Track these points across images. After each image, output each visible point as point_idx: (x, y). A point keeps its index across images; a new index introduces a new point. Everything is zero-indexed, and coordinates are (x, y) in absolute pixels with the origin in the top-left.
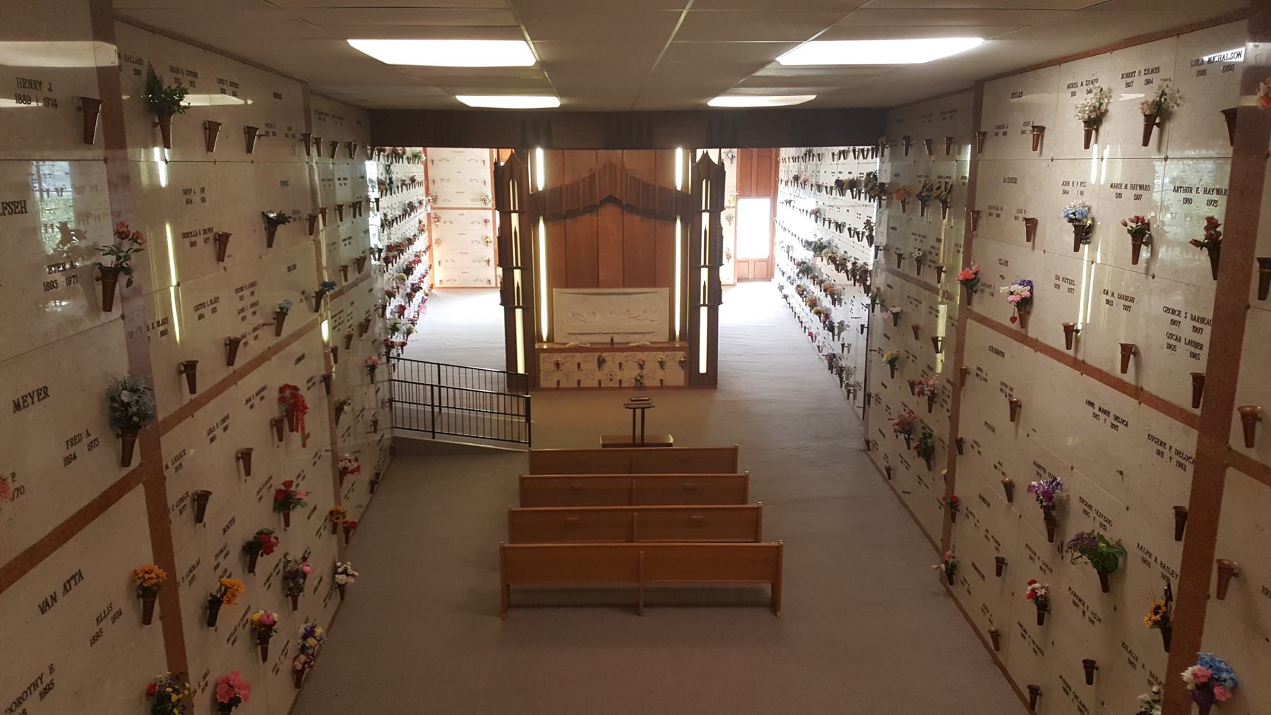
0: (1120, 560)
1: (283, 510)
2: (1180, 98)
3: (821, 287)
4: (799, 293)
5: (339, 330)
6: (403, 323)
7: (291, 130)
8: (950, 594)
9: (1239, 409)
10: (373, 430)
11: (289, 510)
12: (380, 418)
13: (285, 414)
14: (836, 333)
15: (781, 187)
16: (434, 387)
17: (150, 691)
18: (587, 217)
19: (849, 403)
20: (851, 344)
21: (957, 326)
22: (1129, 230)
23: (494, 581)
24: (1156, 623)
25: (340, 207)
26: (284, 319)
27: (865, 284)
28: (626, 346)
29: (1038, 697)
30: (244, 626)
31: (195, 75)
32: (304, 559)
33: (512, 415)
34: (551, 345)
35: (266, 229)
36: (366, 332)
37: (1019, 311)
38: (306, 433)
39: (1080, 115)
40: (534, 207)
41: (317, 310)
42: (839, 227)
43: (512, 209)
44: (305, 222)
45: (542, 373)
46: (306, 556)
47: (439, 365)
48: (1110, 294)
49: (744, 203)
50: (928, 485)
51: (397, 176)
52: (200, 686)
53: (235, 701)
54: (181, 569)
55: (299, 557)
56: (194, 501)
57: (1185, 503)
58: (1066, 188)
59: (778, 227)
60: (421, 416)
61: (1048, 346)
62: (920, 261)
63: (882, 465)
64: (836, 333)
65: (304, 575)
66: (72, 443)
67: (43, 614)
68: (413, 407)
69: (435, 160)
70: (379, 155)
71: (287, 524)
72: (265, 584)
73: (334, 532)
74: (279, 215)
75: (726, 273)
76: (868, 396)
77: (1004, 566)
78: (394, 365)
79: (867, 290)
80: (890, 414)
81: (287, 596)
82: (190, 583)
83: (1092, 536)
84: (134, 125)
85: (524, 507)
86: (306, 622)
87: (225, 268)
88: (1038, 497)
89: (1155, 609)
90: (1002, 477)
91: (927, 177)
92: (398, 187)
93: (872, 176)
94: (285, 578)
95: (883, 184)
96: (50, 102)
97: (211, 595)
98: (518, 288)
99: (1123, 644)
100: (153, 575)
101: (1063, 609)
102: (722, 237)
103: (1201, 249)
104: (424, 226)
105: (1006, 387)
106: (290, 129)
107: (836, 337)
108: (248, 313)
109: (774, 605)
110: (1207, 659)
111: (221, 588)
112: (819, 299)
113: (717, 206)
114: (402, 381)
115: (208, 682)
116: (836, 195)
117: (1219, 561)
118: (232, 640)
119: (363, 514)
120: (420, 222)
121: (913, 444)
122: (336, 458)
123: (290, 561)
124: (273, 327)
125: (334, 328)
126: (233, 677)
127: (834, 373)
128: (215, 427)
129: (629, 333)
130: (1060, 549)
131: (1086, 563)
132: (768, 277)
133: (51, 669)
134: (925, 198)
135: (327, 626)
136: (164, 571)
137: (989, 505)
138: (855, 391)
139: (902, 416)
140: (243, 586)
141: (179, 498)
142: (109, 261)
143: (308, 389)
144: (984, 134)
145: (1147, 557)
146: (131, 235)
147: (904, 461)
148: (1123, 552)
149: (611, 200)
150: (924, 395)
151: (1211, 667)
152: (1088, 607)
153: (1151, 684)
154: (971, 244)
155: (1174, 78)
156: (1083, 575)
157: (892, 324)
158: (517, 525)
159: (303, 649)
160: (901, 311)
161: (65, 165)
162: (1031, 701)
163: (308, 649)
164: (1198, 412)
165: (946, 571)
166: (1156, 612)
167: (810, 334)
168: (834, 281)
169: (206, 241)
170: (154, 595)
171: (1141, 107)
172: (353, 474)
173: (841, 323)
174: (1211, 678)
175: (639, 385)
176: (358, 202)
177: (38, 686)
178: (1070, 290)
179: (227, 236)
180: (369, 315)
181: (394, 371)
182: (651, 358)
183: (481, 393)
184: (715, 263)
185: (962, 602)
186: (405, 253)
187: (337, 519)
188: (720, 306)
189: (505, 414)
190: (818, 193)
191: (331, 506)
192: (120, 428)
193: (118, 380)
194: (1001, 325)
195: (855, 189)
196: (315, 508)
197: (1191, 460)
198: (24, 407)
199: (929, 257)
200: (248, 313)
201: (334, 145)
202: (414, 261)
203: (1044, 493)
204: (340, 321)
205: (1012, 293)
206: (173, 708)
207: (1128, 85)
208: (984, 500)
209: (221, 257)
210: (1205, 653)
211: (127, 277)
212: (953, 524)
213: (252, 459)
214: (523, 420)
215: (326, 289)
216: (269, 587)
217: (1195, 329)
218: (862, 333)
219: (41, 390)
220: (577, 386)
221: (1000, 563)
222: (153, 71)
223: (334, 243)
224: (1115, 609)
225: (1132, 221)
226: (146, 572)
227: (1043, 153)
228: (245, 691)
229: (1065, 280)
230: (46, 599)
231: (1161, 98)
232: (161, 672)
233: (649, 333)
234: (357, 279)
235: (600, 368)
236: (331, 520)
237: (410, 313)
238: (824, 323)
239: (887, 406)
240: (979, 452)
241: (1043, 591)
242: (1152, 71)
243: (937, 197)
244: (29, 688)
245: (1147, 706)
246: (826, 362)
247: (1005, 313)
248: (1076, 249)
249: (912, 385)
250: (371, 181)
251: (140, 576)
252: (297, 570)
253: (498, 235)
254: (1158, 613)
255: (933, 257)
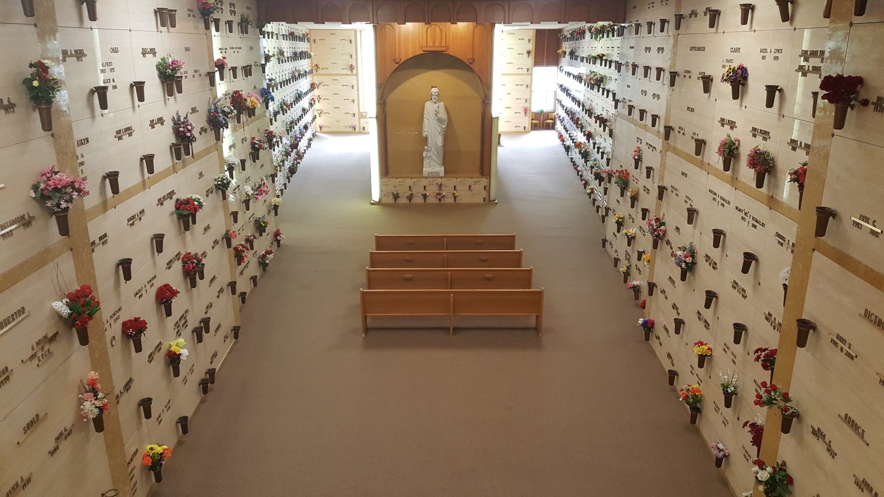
109: (537, 329)
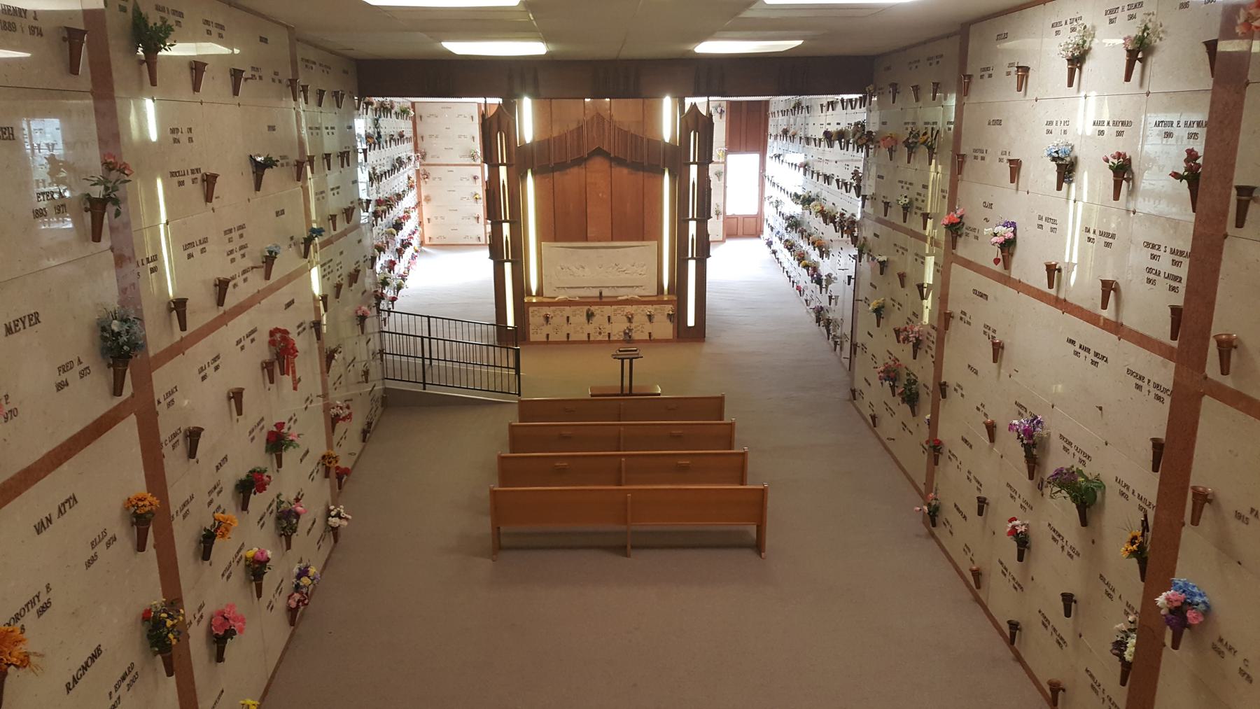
0: (1099, 494)
1: (275, 452)
2: (1163, 32)
3: (809, 239)
4: (787, 247)
5: (328, 279)
6: (394, 278)
7: (277, 75)
8: (933, 535)
9: (1214, 337)
10: (364, 380)
11: (281, 451)
12: (372, 371)
13: (275, 357)
14: (824, 286)
15: (770, 141)
16: (424, 339)
17: (146, 616)
18: (575, 170)
19: (836, 355)
20: (838, 296)
21: (942, 272)
22: (1110, 166)
23: (485, 525)
24: (1133, 553)
25: (328, 156)
26: (273, 263)
27: (852, 235)
28: (614, 300)
29: (1018, 632)
30: (238, 562)
31: (181, 15)
32: (297, 500)
33: (501, 367)
34: (540, 299)
35: (254, 173)
36: (356, 282)
37: (1002, 252)
38: (297, 378)
39: (1063, 53)
40: (522, 160)
41: (306, 256)
42: (827, 179)
43: (500, 162)
44: (293, 168)
45: (531, 327)
46: (300, 497)
47: (429, 317)
48: (1092, 231)
49: (733, 159)
50: (911, 430)
51: (385, 130)
52: (195, 618)
53: (230, 633)
54: (175, 504)
55: (292, 499)
56: (200, 543)
57: (1162, 435)
58: (1050, 128)
59: (767, 184)
60: (412, 368)
61: (1031, 287)
62: (906, 208)
63: (867, 412)
64: (824, 286)
65: (298, 515)
66: (64, 369)
67: (38, 534)
68: (404, 359)
69: (423, 115)
70: (367, 109)
71: (280, 465)
72: (259, 522)
73: (327, 475)
74: (266, 159)
75: (715, 227)
76: (854, 347)
77: (985, 505)
78: (385, 319)
79: (855, 241)
80: (875, 362)
81: (281, 535)
82: (184, 517)
83: (1071, 471)
84: (122, 65)
85: (514, 453)
86: (300, 562)
87: (213, 210)
88: (1019, 435)
89: (1132, 539)
90: (984, 419)
91: (914, 123)
92: (386, 142)
93: (859, 126)
94: (278, 518)
95: (870, 133)
96: (36, 30)
97: (205, 529)
98: (507, 238)
99: (1101, 576)
100: (146, 503)
101: (1043, 545)
102: (710, 189)
103: (1181, 181)
104: (413, 182)
105: (989, 329)
106: (276, 74)
107: (824, 290)
108: (237, 255)
109: (758, 546)
110: (1181, 584)
111: (215, 523)
112: (807, 253)
113: (705, 158)
114: (392, 333)
115: (203, 615)
116: (825, 146)
117: (1194, 488)
118: (227, 574)
119: (356, 462)
120: (409, 178)
121: (898, 391)
122: (327, 408)
123: (283, 502)
124: (262, 271)
125: (324, 277)
126: (228, 610)
127: (821, 325)
128: (207, 366)
129: (618, 287)
130: (1040, 487)
131: (1065, 497)
132: (757, 234)
133: (48, 588)
134: (912, 145)
135: (321, 566)
136: (157, 499)
137: (971, 447)
138: (841, 342)
139: (887, 363)
140: (236, 520)
141: (172, 433)
142: (98, 192)
143: (299, 334)
144: (970, 77)
145: (1124, 490)
146: (118, 166)
147: (889, 409)
148: (1102, 486)
149: (599, 152)
150: (909, 342)
151: (1184, 591)
152: (1067, 542)
153: (1127, 614)
154: (957, 187)
155: (1157, 13)
156: (1061, 509)
157: (879, 272)
158: (508, 470)
159: (297, 588)
160: (888, 259)
161: (56, 122)
162: (1011, 636)
163: (302, 588)
164: (1175, 344)
165: (929, 514)
166: (1132, 543)
167: (798, 288)
168: (822, 233)
169: (194, 181)
170: (148, 523)
171: (1124, 42)
172: (344, 421)
173: (829, 276)
174: (1185, 603)
175: (628, 337)
176: (345, 152)
177: (35, 604)
178: (1053, 230)
179: (215, 177)
180: (359, 266)
181: (385, 325)
182: (640, 312)
183: (471, 345)
184: (704, 215)
185: (944, 543)
186: (394, 209)
187: (330, 463)
188: (707, 259)
189: (495, 366)
190: (807, 146)
191: (324, 450)
192: (111, 357)
193: (109, 311)
194: (985, 267)
195: (843, 140)
196: (307, 452)
197: (1169, 393)
198: (16, 331)
199: (915, 204)
200: (237, 255)
201: (321, 93)
202: (404, 216)
203: (1025, 431)
204: (330, 270)
205: (995, 235)
206: (168, 633)
207: (1111, 21)
208: (966, 441)
209: (208, 198)
210: (1179, 579)
211: (115, 208)
212: (936, 467)
213: (243, 400)
214: (513, 372)
215: (314, 235)
216: (262, 526)
217: (1175, 263)
218: (849, 284)
219: (32, 315)
220: (566, 339)
221: (982, 502)
222: (138, 8)
223: (322, 192)
224: (1093, 542)
225: (1114, 158)
226: (140, 500)
227: (1028, 94)
228: (240, 623)
229: (1048, 219)
230: (42, 520)
231: (1143, 33)
232: (156, 599)
233: (637, 287)
234: (346, 229)
235: (589, 321)
236: (323, 465)
237: (400, 268)
238: (812, 276)
239: (873, 355)
240: (962, 395)
241: (1023, 528)
242: (1135, 6)
243: (924, 143)
244: (27, 605)
245: (1123, 635)
246: (813, 315)
247: (988, 254)
248: (1059, 188)
249: (897, 332)
250: (360, 136)
251: (133, 503)
252: (290, 510)
253: (486, 179)
254: (1135, 543)
255: (919, 204)
